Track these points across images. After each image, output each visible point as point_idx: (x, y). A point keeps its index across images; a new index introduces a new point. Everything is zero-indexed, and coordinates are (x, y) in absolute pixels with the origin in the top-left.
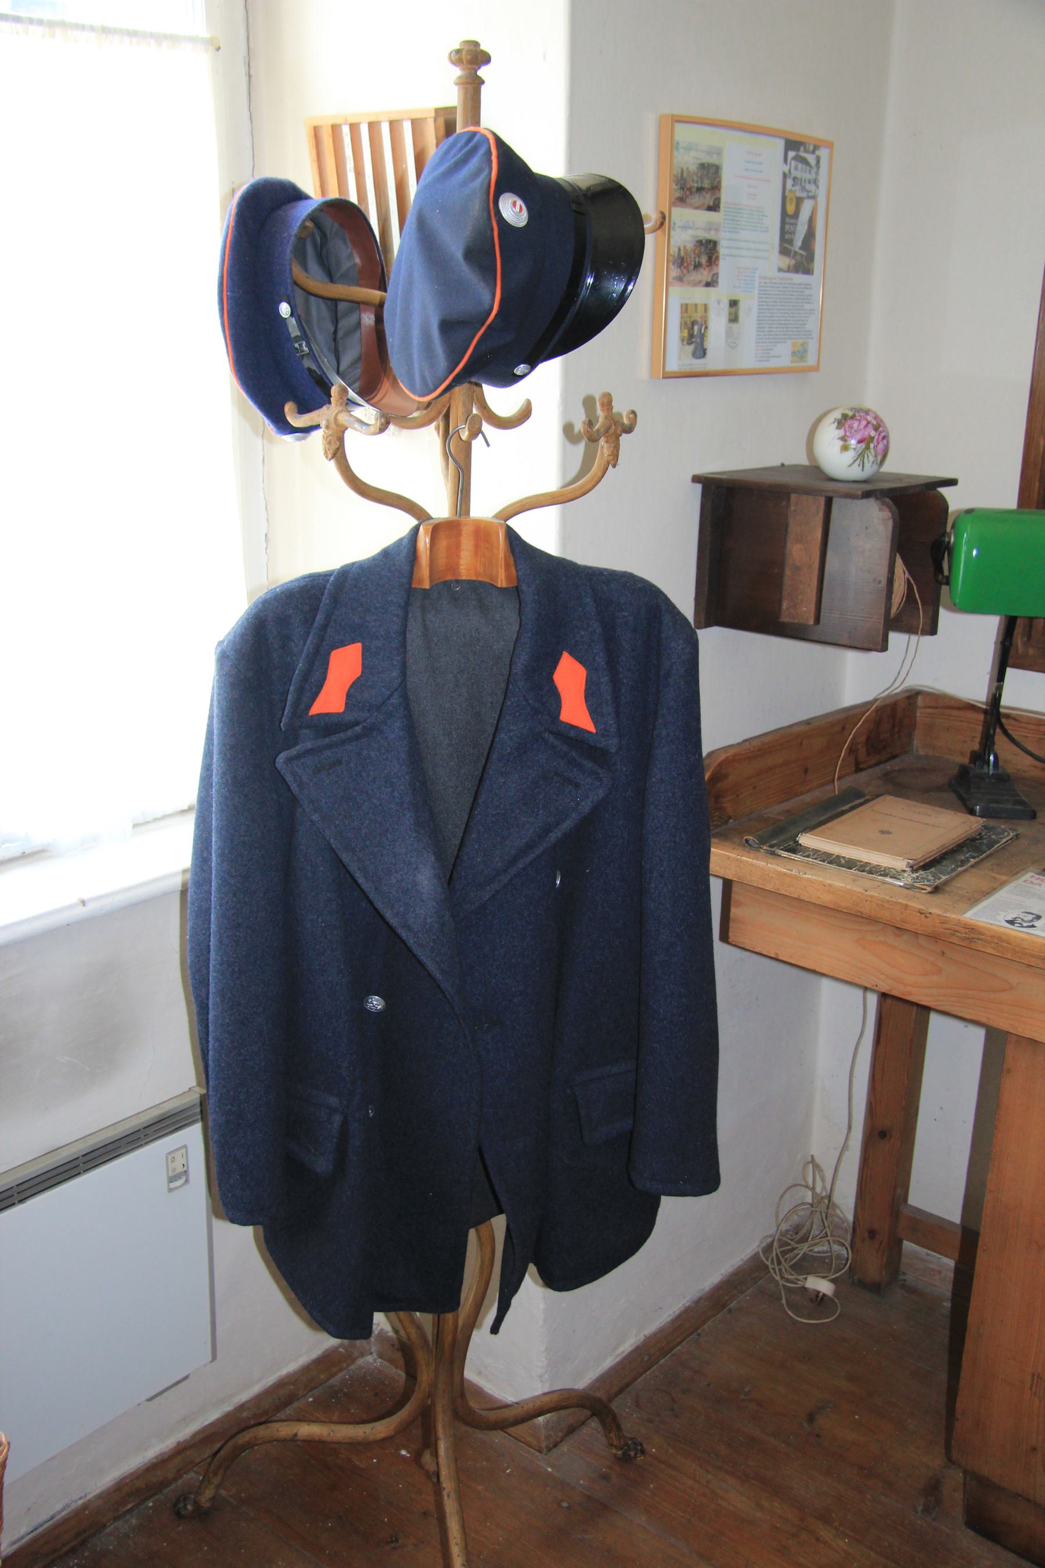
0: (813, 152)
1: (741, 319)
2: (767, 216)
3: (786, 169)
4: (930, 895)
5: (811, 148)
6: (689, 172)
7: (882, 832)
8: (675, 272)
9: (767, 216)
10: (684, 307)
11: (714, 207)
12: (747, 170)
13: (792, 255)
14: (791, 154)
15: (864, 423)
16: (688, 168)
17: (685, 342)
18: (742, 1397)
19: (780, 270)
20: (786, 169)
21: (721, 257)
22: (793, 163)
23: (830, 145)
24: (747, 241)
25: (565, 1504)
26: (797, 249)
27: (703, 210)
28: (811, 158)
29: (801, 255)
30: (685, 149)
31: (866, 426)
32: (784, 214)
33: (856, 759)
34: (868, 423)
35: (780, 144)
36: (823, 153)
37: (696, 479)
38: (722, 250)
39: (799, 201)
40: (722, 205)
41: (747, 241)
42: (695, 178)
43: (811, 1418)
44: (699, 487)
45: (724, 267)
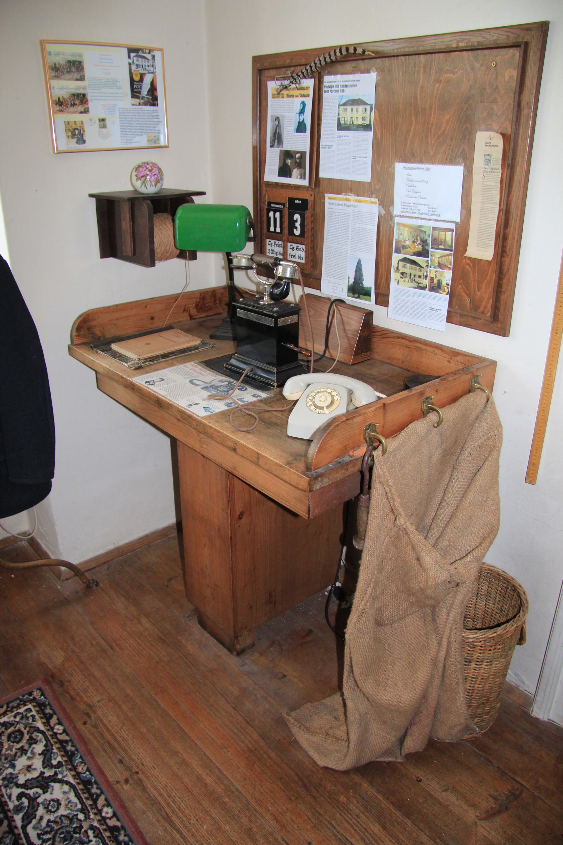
0: (149, 53)
1: (107, 126)
2: (119, 82)
3: (131, 61)
4: (135, 371)
5: (147, 51)
6: (60, 65)
7: (147, 344)
8: (58, 108)
9: (119, 82)
10: (67, 123)
11: (82, 79)
12: (101, 62)
13: (141, 98)
14: (132, 55)
15: (145, 168)
16: (59, 63)
17: (70, 138)
18: (150, 570)
19: (133, 105)
20: (131, 61)
21: (89, 100)
22: (135, 59)
23: (161, 50)
24: (108, 93)
25: (56, 600)
26: (144, 96)
27: (73, 80)
28: (149, 56)
29: (148, 98)
30: (55, 55)
31: (145, 170)
32: (132, 80)
33: (189, 314)
34: (147, 168)
35: (126, 50)
36: (157, 54)
37: (91, 196)
38: (89, 97)
39: (142, 76)
40: (86, 78)
41: (108, 93)
42: (65, 67)
43: (170, 580)
44: (94, 200)
45: (91, 105)
